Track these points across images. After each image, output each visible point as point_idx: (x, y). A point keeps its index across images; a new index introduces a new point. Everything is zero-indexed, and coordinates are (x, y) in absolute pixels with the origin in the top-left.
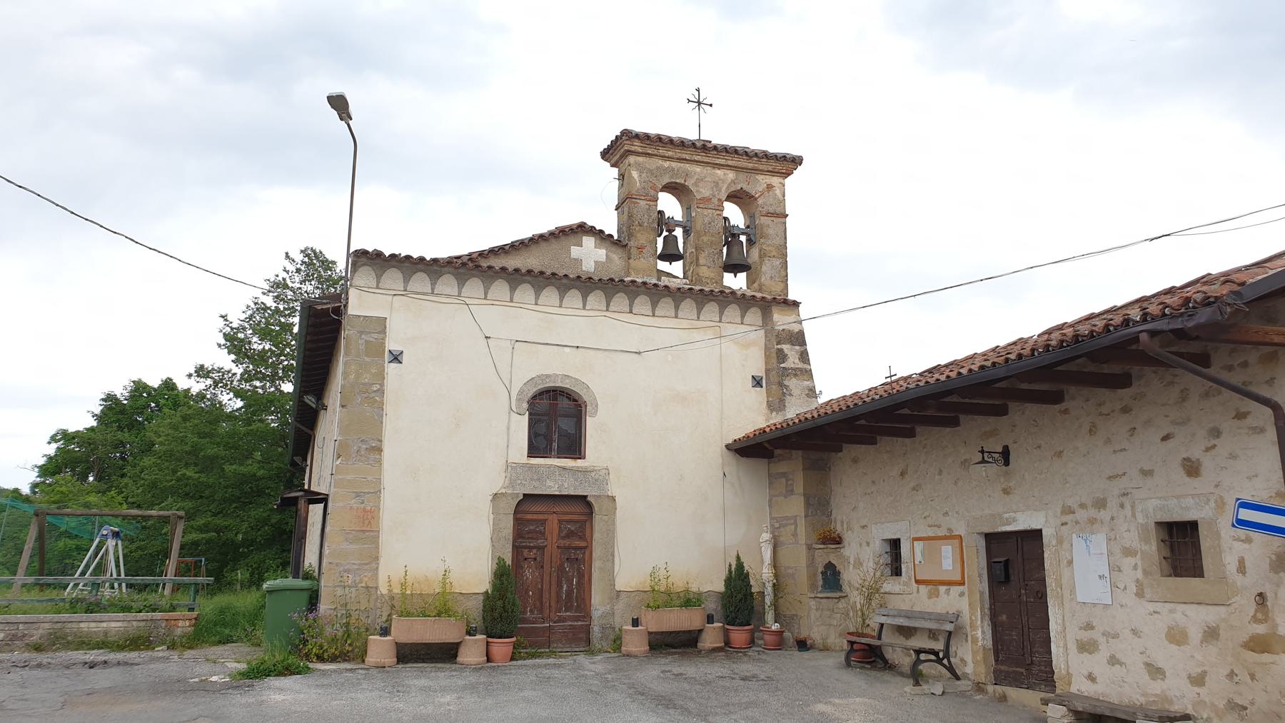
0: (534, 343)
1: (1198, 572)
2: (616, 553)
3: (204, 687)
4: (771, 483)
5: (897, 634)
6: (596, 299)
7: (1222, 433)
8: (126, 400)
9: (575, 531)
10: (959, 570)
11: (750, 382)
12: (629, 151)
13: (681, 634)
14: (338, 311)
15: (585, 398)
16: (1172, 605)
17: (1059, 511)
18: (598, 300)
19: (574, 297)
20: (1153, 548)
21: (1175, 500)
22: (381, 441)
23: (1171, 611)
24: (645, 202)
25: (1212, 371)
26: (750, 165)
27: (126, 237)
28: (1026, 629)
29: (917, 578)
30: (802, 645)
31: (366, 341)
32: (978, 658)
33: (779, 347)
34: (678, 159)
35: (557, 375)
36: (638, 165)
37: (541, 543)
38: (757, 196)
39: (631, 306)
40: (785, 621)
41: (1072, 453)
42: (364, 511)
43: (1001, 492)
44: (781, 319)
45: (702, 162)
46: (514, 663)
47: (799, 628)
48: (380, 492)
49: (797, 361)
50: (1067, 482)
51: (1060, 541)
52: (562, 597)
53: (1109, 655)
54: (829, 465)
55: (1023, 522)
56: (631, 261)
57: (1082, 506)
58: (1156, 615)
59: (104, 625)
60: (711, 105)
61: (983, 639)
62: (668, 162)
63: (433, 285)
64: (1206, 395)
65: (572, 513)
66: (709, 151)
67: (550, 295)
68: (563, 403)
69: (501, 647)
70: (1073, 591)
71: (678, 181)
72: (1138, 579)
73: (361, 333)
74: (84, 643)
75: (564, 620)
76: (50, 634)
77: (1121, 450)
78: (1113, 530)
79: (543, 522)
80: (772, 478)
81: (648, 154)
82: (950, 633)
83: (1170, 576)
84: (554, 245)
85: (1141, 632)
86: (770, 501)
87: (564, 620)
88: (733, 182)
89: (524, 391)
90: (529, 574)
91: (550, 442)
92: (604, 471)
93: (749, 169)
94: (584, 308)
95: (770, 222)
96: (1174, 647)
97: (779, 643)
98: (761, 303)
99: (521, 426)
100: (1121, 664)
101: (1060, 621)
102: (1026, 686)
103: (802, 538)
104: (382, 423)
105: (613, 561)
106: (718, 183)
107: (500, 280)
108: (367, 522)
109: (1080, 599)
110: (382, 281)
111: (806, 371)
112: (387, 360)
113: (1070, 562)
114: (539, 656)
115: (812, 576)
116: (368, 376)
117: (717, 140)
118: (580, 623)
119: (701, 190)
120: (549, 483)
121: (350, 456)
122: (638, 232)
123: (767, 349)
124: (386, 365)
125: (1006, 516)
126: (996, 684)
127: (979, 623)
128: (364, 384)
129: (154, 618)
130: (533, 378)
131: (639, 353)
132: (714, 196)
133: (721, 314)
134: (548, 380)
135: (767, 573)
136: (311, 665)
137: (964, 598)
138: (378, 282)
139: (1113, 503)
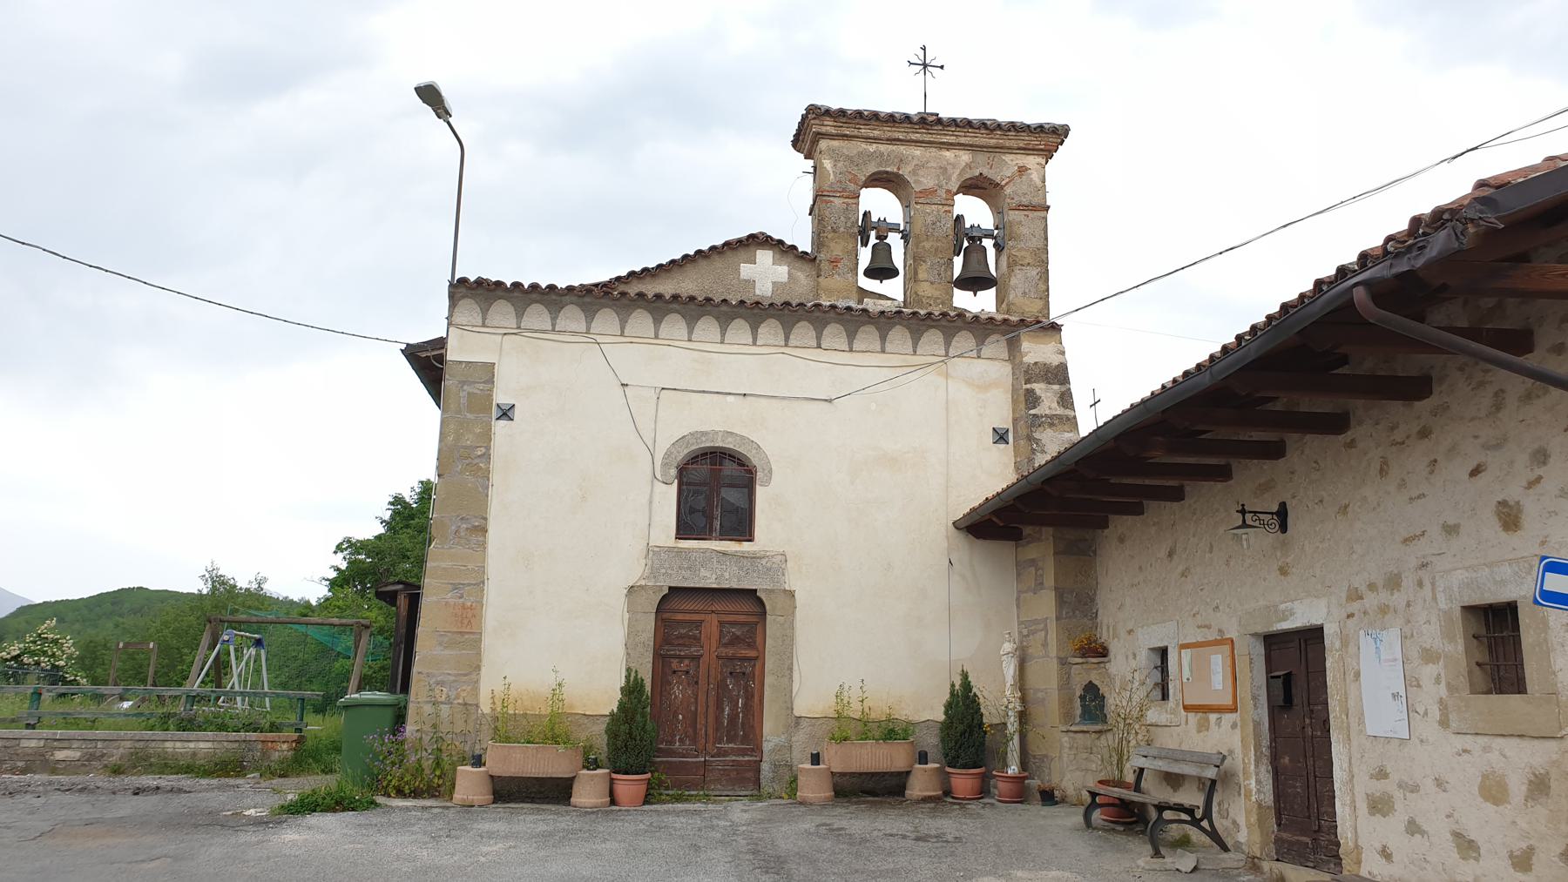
0: (686, 390)
1: (1519, 687)
2: (795, 667)
3: (236, 823)
4: (1019, 575)
5: (1164, 783)
6: (770, 331)
7: (1550, 456)
8: (416, 503)
9: (742, 637)
10: (1230, 690)
11: (990, 437)
12: (819, 134)
13: (886, 777)
14: (441, 359)
15: (755, 461)
16: (1486, 739)
17: (1344, 595)
18: (773, 332)
19: (739, 330)
20: (1457, 648)
21: (1487, 569)
22: (486, 519)
23: (1486, 749)
24: (842, 200)
25: (1531, 360)
26: (993, 142)
27: (44, 250)
28: (1311, 779)
29: (1185, 703)
30: (1048, 797)
31: (469, 393)
32: (1252, 820)
33: (1028, 386)
34: (888, 140)
35: (717, 432)
36: (832, 150)
37: (695, 651)
38: (1003, 183)
39: (819, 338)
40: (1034, 763)
41: (1360, 507)
42: (464, 607)
43: (1278, 572)
44: (1035, 351)
45: (922, 142)
46: (646, 807)
47: (1050, 774)
48: (483, 583)
49: (1055, 405)
50: (1353, 552)
51: (1345, 643)
52: (723, 723)
53: (1407, 818)
54: (1094, 548)
55: (1301, 616)
56: (820, 279)
57: (1372, 587)
58: (1466, 756)
59: (192, 745)
60: (942, 67)
61: (1259, 791)
62: (875, 145)
63: (554, 319)
64: (1528, 397)
65: (737, 613)
66: (931, 126)
67: (707, 328)
68: (729, 468)
69: (630, 786)
70: (1361, 721)
71: (888, 169)
72: (1441, 699)
73: (463, 383)
74: (168, 766)
75: (725, 753)
76: (132, 754)
77: (1419, 497)
78: (1409, 622)
79: (698, 624)
80: (1020, 567)
81: (846, 136)
82: (1213, 782)
83: (1489, 692)
84: (718, 263)
85: (1447, 782)
86: (1018, 599)
87: (725, 753)
88: (968, 166)
89: (672, 453)
90: (678, 692)
91: (710, 518)
92: (780, 557)
93: (991, 147)
94: (754, 343)
95: (1022, 218)
96: (1490, 807)
97: (1020, 794)
98: (1003, 327)
99: (668, 496)
100: (1423, 833)
101: (1345, 765)
102: (1312, 865)
103: (1053, 650)
104: (487, 496)
105: (791, 677)
106: (946, 169)
107: (639, 310)
108: (466, 622)
109: (1370, 732)
110: (489, 316)
111: (1068, 419)
112: (494, 415)
113: (1357, 675)
114: (687, 800)
115: (1066, 703)
116: (471, 436)
117: (945, 114)
118: (747, 758)
119: (922, 179)
120: (703, 572)
121: (447, 539)
122: (832, 239)
123: (1014, 390)
124: (493, 423)
125: (1282, 607)
126: (1278, 860)
127: (1252, 767)
128: (466, 447)
129: (248, 739)
130: (684, 437)
131: (830, 401)
132: (941, 187)
133: (948, 344)
134: (704, 439)
135: (1010, 695)
136: (380, 800)
137: (1236, 730)
138: (484, 319)
139: (1408, 581)
